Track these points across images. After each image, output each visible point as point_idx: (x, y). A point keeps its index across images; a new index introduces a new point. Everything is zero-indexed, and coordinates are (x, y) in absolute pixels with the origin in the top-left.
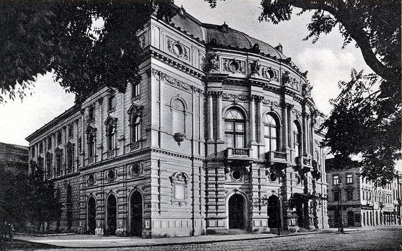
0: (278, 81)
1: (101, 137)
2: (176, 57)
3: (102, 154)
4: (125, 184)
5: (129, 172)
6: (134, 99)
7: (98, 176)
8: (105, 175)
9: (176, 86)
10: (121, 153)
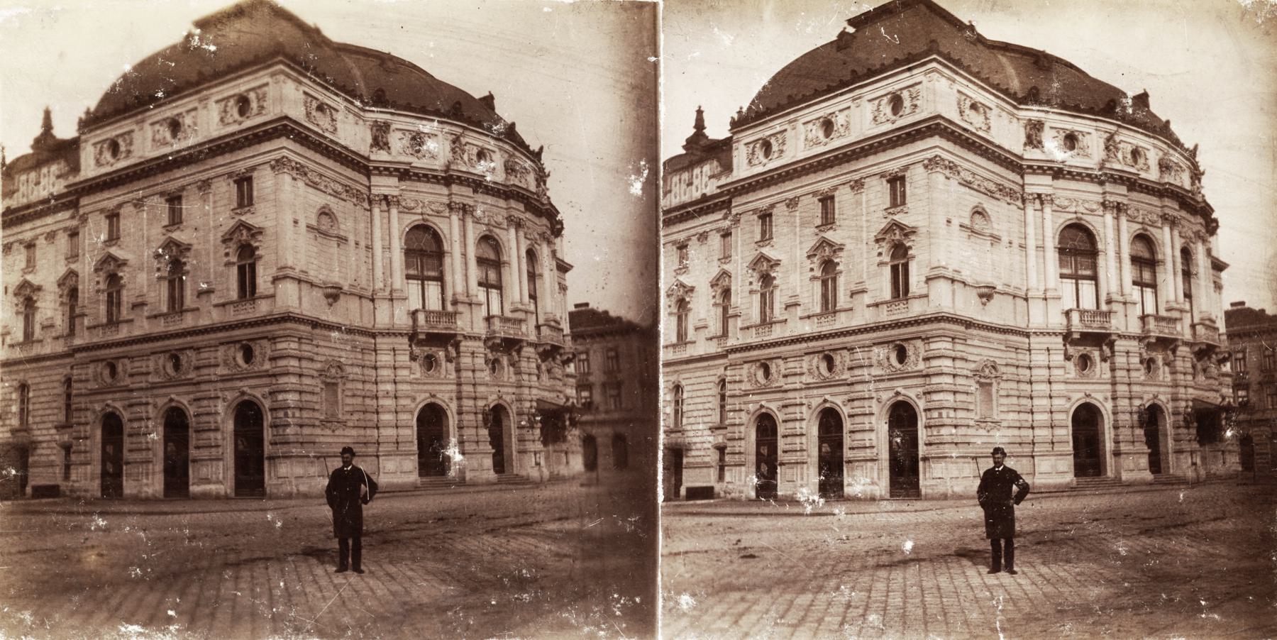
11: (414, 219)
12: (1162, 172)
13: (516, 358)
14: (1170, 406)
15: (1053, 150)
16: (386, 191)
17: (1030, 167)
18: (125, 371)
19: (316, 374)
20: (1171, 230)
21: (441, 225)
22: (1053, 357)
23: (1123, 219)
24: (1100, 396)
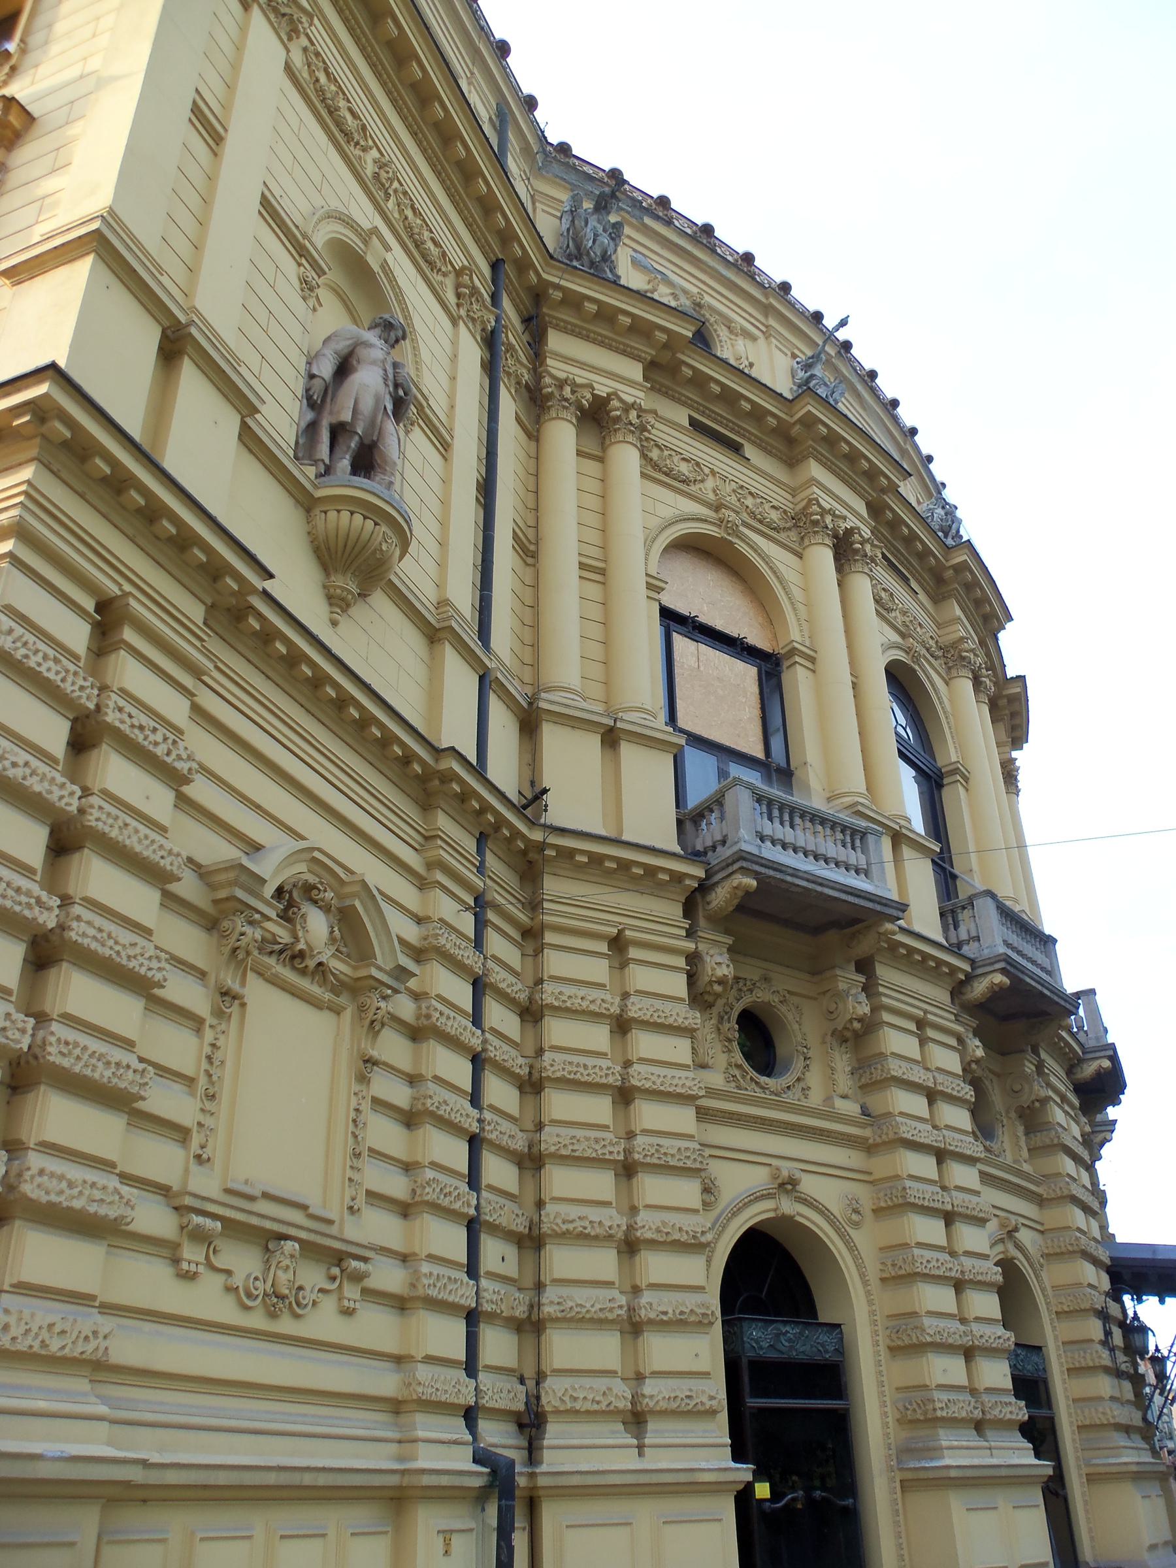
22: (641, 978)
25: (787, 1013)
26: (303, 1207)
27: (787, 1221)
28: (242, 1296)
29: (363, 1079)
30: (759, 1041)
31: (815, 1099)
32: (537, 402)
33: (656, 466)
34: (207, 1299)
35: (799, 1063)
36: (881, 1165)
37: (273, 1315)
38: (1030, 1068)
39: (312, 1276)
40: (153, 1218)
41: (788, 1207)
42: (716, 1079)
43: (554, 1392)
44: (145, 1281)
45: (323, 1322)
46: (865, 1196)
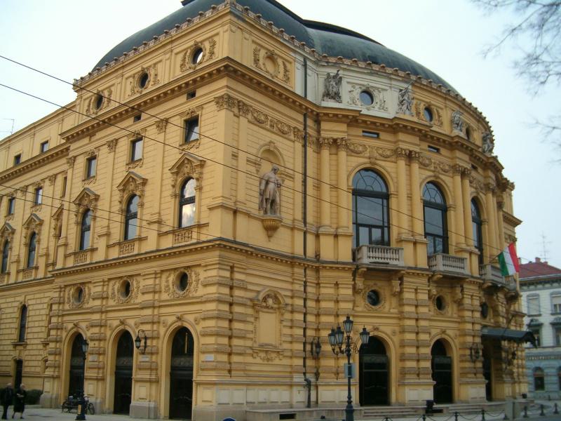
0: (461, 130)
1: (108, 215)
2: (271, 78)
3: (108, 247)
4: (104, 315)
5: (113, 293)
6: (131, 166)
7: (96, 290)
8: (67, 294)
9: (268, 127)
10: (99, 256)
11: (361, 161)
12: (452, 127)
13: (460, 295)
14: (396, 339)
15: (349, 99)
16: (336, 135)
17: (327, 115)
18: (90, 294)
19: (249, 303)
20: (462, 178)
21: (387, 167)
22: (342, 291)
23: (415, 166)
24: (388, 330)
25: (445, 297)
26: (271, 345)
27: (444, 339)
28: (263, 359)
29: (281, 323)
30: (440, 303)
31: (450, 314)
32: (319, 145)
33: (352, 151)
34: (258, 360)
35: (383, 302)
36: (461, 326)
37: (268, 361)
38: (495, 297)
39: (274, 355)
40: (249, 351)
41: (444, 336)
42: (432, 313)
43: (234, 366)
44: (249, 359)
45: (277, 361)
46: (458, 333)
